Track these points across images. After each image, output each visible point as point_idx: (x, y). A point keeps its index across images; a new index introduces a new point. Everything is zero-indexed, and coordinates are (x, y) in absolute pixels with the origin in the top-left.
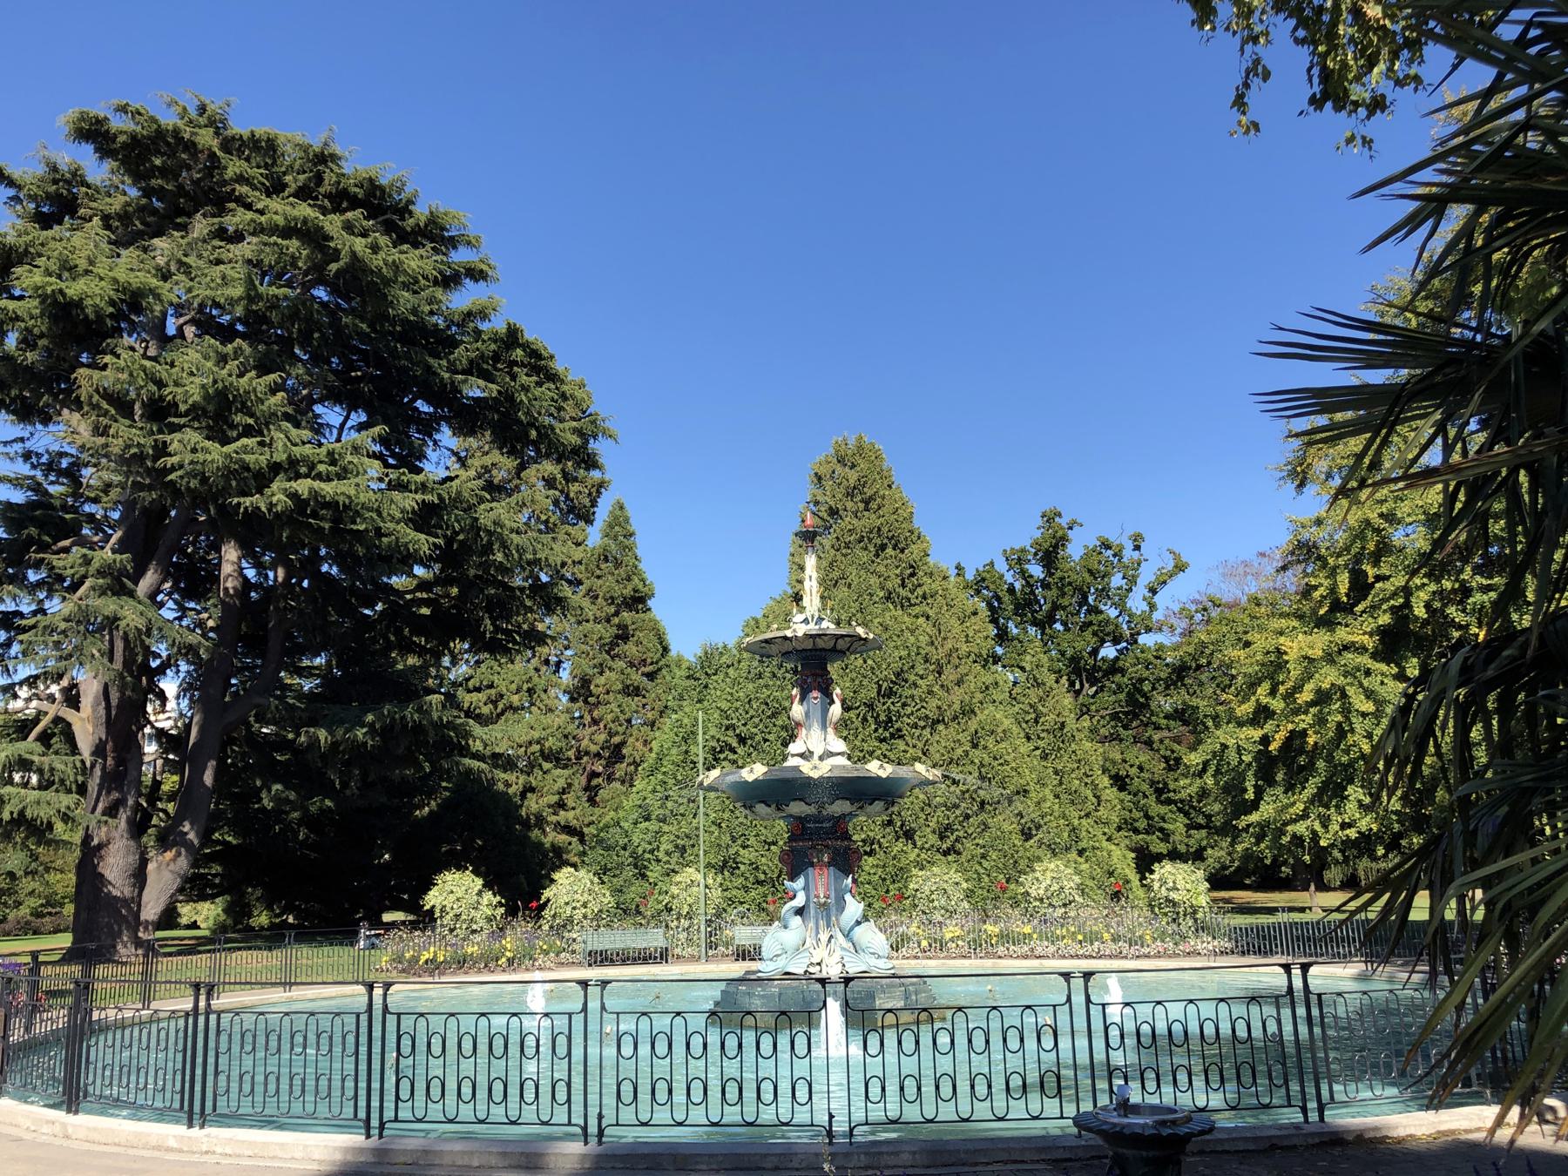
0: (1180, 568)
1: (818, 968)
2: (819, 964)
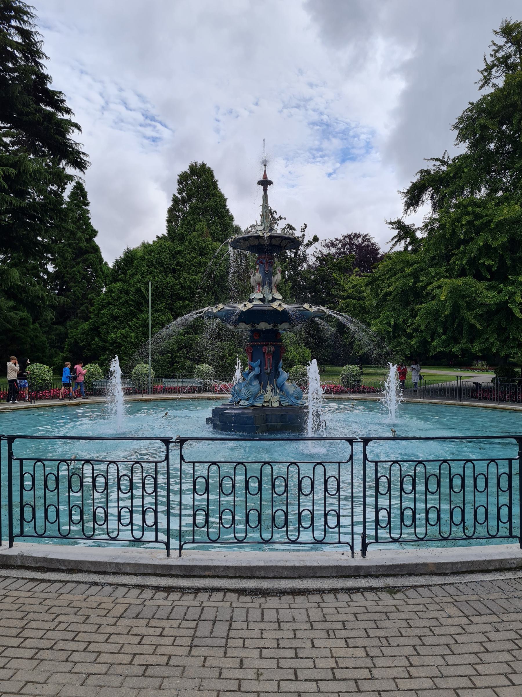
0: (316, 239)
1: (268, 404)
2: (268, 402)
